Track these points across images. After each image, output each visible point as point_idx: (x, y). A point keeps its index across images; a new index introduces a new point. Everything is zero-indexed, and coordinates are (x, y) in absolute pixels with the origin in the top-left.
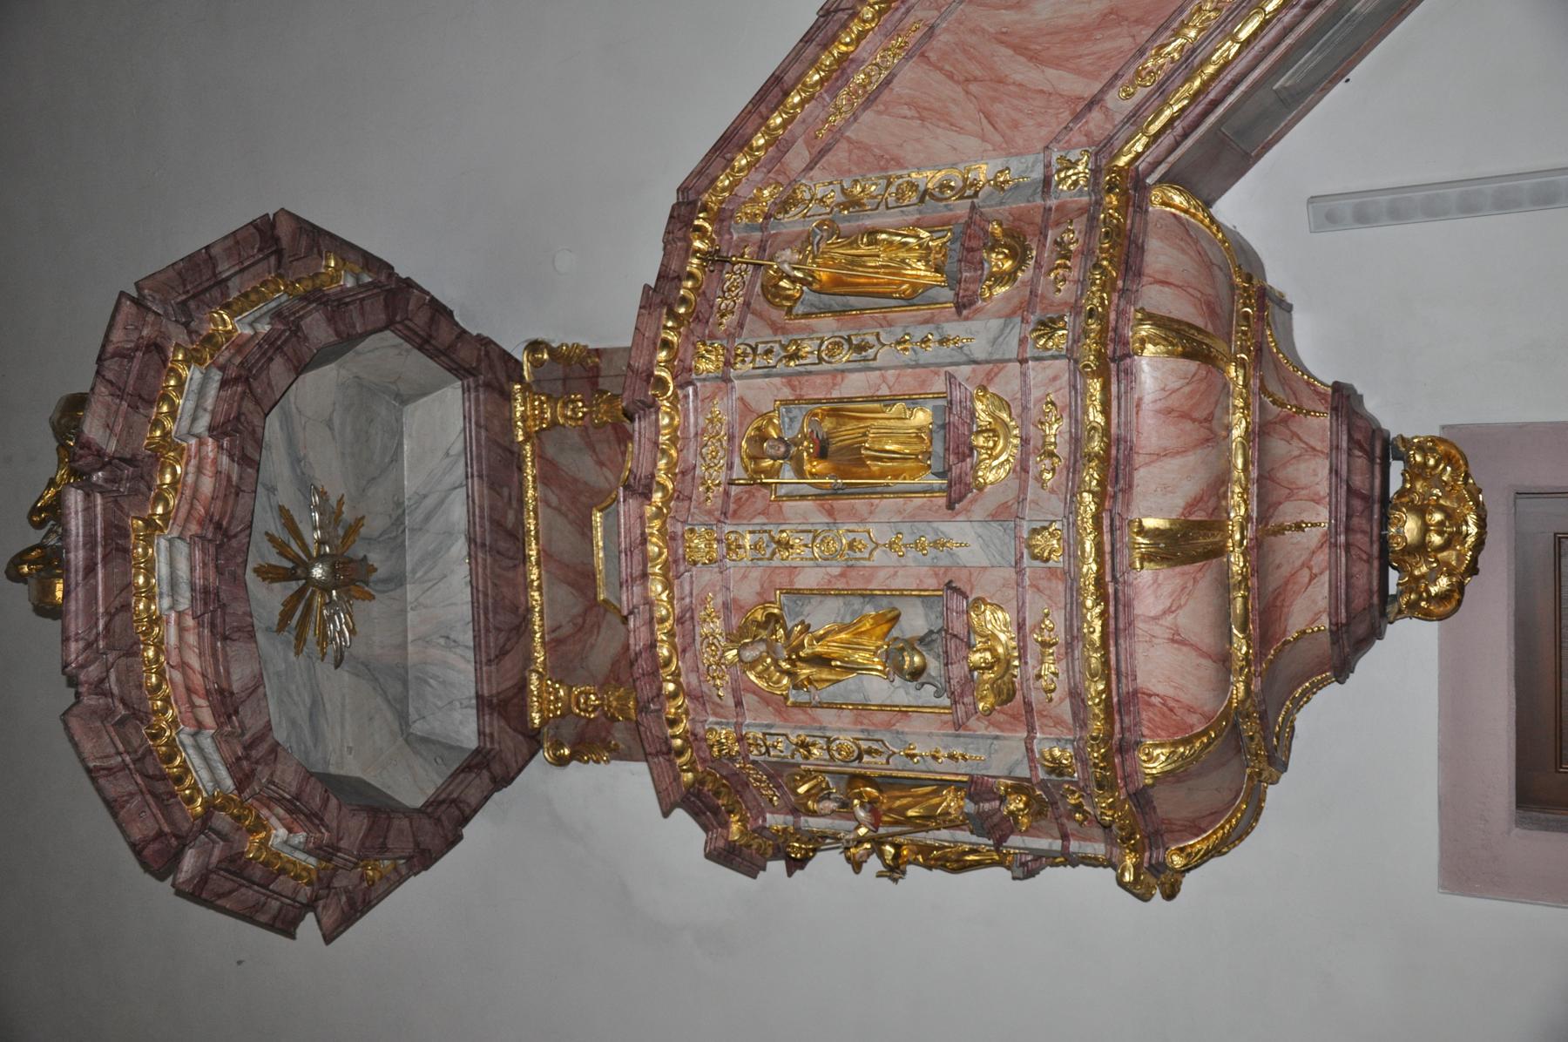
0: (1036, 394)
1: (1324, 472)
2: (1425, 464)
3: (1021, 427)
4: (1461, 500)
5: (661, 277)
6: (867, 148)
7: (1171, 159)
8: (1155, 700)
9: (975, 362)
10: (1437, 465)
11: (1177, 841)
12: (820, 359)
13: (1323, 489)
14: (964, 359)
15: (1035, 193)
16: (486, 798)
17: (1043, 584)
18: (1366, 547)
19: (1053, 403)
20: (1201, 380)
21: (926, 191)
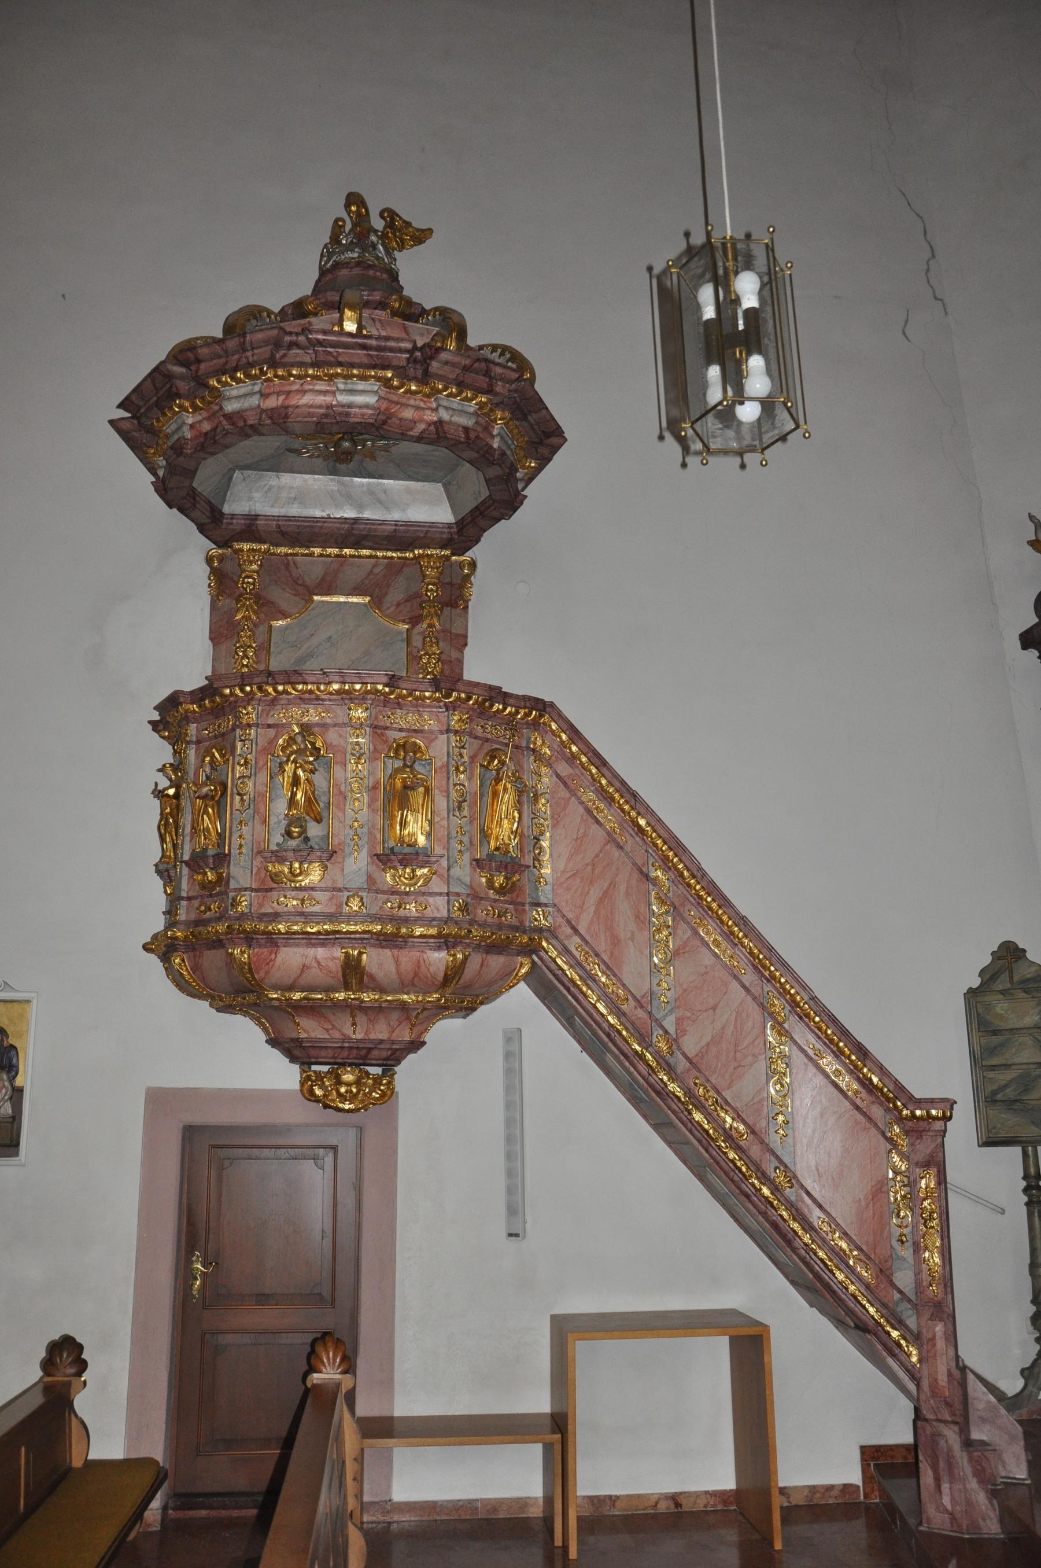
0: (431, 900)
1: (381, 1036)
2: (381, 1084)
3: (414, 893)
4: (362, 1101)
5: (506, 694)
6: (564, 809)
7: (544, 967)
8: (273, 956)
9: (449, 869)
10: (380, 1090)
11: (188, 959)
12: (455, 785)
13: (372, 1036)
14: (451, 863)
15: (532, 898)
16: (193, 521)
17: (334, 901)
18: (341, 1056)
19: (426, 908)
20: (433, 982)
21: (539, 840)
